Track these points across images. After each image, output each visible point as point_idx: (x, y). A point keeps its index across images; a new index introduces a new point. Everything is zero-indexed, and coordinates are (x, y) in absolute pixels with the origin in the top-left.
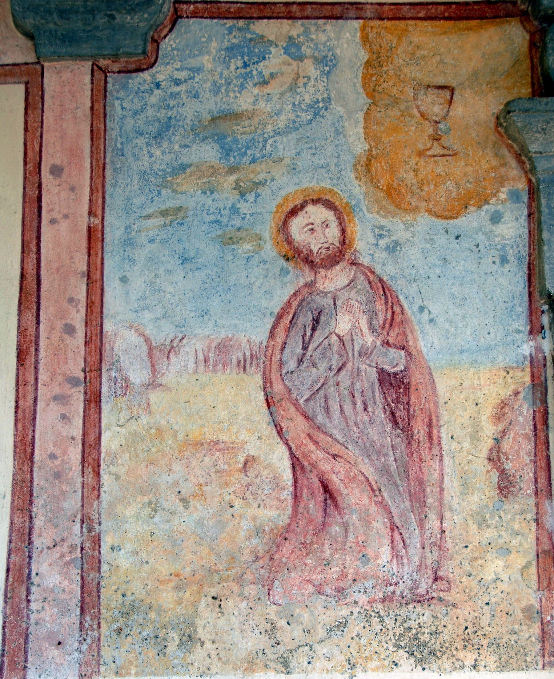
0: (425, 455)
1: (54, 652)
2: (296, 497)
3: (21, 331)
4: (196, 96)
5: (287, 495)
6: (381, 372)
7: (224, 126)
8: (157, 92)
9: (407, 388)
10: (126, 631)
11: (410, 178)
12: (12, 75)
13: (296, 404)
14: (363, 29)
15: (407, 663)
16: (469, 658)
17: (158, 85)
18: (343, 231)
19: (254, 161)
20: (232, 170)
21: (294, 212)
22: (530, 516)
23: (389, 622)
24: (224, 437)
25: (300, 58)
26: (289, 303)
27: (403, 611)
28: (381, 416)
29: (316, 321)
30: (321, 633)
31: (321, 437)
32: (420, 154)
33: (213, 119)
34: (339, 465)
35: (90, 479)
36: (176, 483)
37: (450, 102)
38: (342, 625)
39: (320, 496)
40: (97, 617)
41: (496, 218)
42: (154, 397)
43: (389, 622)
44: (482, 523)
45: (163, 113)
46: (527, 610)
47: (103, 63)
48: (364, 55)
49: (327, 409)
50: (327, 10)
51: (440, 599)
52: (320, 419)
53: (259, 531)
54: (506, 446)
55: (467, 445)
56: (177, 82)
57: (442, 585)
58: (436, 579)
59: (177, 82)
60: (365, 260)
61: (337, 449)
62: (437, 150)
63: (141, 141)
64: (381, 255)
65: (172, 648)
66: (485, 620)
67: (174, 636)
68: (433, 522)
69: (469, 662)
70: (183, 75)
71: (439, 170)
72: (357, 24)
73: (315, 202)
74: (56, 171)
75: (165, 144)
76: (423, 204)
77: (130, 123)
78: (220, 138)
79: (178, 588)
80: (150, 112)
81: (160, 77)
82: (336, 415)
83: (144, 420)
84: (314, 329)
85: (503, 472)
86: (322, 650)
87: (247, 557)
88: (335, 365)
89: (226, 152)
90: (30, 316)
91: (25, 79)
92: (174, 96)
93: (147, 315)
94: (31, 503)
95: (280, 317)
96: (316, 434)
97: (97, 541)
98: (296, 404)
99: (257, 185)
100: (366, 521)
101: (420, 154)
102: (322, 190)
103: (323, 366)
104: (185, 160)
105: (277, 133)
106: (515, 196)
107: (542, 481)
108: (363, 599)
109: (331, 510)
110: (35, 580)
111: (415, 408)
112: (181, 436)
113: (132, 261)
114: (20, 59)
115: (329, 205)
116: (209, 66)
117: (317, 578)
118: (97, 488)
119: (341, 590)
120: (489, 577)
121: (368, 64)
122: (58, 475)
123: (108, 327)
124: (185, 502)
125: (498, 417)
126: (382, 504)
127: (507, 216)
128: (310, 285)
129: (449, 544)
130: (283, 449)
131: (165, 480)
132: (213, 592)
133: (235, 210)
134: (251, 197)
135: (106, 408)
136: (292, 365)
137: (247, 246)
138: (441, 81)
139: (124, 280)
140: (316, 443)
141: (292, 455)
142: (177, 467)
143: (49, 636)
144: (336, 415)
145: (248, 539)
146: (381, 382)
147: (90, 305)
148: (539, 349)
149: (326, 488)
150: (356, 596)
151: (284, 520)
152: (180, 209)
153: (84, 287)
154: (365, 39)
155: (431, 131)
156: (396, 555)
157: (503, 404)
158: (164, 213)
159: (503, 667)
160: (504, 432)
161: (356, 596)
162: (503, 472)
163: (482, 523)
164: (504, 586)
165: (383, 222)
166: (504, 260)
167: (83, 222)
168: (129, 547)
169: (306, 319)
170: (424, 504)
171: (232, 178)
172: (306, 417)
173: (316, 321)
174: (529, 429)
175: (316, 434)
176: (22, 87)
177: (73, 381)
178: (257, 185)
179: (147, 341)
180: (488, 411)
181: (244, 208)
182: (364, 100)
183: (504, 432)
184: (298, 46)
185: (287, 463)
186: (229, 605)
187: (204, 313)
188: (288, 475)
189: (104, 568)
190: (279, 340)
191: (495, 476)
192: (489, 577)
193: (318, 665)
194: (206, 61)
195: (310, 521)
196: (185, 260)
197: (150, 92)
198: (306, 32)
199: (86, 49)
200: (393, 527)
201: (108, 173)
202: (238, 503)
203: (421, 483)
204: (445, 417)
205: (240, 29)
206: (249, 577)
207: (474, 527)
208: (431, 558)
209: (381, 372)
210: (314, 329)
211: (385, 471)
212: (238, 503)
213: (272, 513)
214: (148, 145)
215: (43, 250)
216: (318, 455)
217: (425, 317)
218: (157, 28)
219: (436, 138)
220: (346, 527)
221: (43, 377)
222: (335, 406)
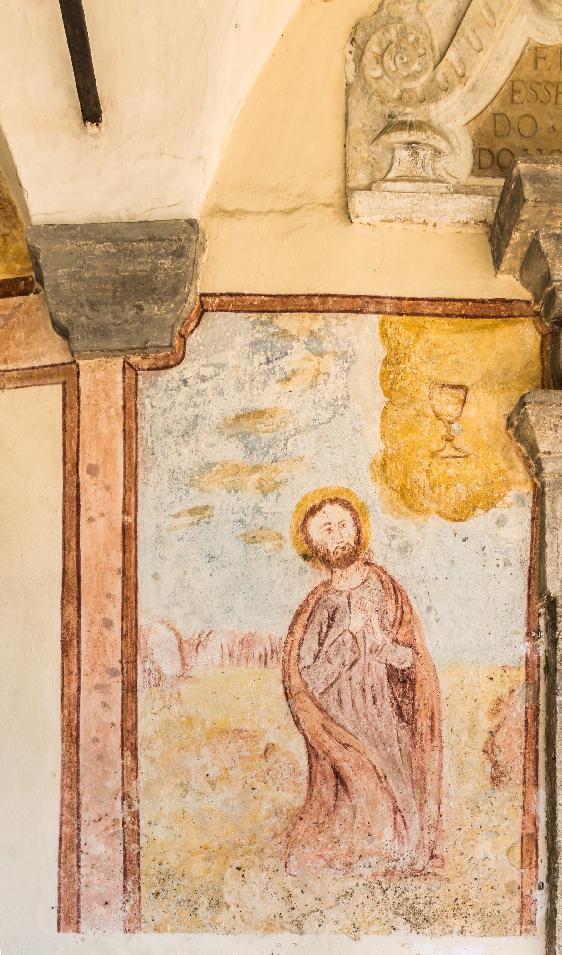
0: (427, 746)
1: (102, 910)
2: (311, 783)
3: (65, 625)
4: (221, 393)
5: (303, 779)
7: (246, 424)
8: (184, 389)
9: (413, 683)
10: (163, 894)
12: (51, 376)
13: (312, 697)
15: (403, 928)
16: (457, 924)
17: (185, 382)
19: (275, 460)
20: (256, 469)
21: (312, 512)
22: (518, 803)
24: (247, 727)
26: (307, 601)
28: (388, 709)
29: (332, 618)
30: (331, 901)
31: (334, 728)
32: (433, 455)
33: (238, 418)
34: (349, 754)
35: (129, 761)
36: (205, 767)
37: (464, 402)
38: (348, 894)
39: (332, 783)
40: (138, 882)
41: (501, 522)
42: (185, 687)
44: (476, 808)
47: (134, 359)
48: (382, 353)
49: (340, 702)
50: (346, 304)
52: (334, 711)
53: (277, 812)
55: (464, 737)
58: (432, 857)
59: (204, 379)
60: (378, 560)
62: (449, 451)
63: (170, 440)
64: (394, 556)
65: (202, 911)
66: (473, 893)
67: (204, 900)
68: (431, 807)
69: (457, 928)
70: (208, 372)
71: (451, 472)
72: (376, 319)
74: (92, 470)
75: (192, 442)
76: (434, 506)
77: (159, 420)
78: (244, 436)
80: (178, 410)
81: (187, 374)
83: (176, 708)
84: (329, 627)
85: (495, 764)
90: (71, 610)
91: (62, 379)
92: (200, 393)
94: (78, 781)
95: (298, 614)
96: (329, 725)
97: (136, 816)
98: (312, 697)
99: (278, 484)
100: (373, 804)
102: (340, 490)
103: (336, 661)
104: (212, 459)
106: (520, 500)
108: (367, 872)
109: (342, 794)
110: (83, 848)
111: (420, 703)
114: (58, 361)
115: (346, 505)
116: (233, 362)
118: (135, 770)
120: (479, 856)
121: (386, 362)
122: (100, 757)
123: (142, 621)
124: (212, 783)
125: (494, 712)
126: (386, 789)
128: (326, 584)
129: (445, 827)
130: (301, 738)
131: (193, 763)
133: (258, 510)
135: (141, 696)
136: (308, 660)
137: (269, 545)
138: (456, 380)
139: (156, 577)
140: (329, 733)
141: (308, 743)
143: (97, 896)
145: (268, 817)
146: (390, 677)
147: (125, 600)
149: (337, 774)
150: (363, 870)
151: (299, 802)
152: (206, 508)
153: (120, 583)
154: (384, 334)
155: (444, 431)
156: (398, 835)
157: (500, 701)
159: (485, 932)
161: (363, 870)
162: (495, 764)
163: (476, 808)
164: (491, 864)
167: (118, 518)
168: (164, 822)
169: (322, 616)
172: (321, 709)
173: (332, 618)
175: (329, 725)
176: (60, 387)
177: (113, 673)
178: (278, 484)
179: (178, 635)
180: (485, 706)
182: (381, 399)
184: (319, 341)
185: (303, 751)
186: (251, 875)
188: (303, 762)
190: (298, 635)
191: (488, 767)
193: (327, 927)
199: (116, 343)
200: (396, 811)
201: (140, 472)
202: (259, 786)
203: (422, 771)
204: (446, 711)
205: (263, 324)
206: (268, 851)
207: (467, 812)
208: (428, 838)
210: (329, 627)
211: (390, 760)
212: (259, 786)
213: (290, 796)
215: (82, 548)
216: (330, 744)
217: (432, 614)
218: (185, 324)
220: (354, 810)
221: (85, 667)
222: (347, 699)
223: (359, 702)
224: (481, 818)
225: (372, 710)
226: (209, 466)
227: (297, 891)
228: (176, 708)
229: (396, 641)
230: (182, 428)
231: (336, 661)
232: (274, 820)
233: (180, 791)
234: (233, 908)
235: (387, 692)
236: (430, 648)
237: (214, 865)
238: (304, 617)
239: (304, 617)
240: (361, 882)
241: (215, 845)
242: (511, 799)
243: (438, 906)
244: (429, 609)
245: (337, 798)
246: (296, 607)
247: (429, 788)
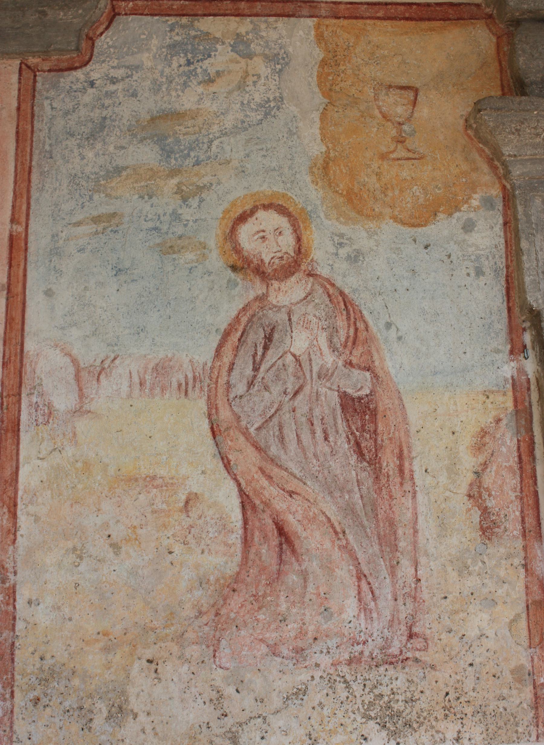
0: (396, 491)
2: (246, 542)
5: (236, 538)
6: (344, 397)
8: (90, 91)
9: (374, 414)
10: (44, 701)
11: (372, 182)
13: (246, 433)
14: (317, 27)
18: (299, 239)
20: (174, 172)
21: (243, 218)
23: (357, 688)
24: (162, 472)
25: (250, 56)
27: (373, 675)
29: (269, 339)
30: (276, 702)
32: (383, 157)
33: (153, 119)
34: (296, 504)
36: (106, 525)
37: (414, 103)
39: (275, 541)
43: (357, 688)
45: (96, 114)
46: (517, 671)
47: (32, 61)
48: (319, 54)
49: (282, 439)
51: (417, 660)
52: (274, 450)
53: (203, 582)
54: (488, 480)
55: (443, 479)
56: (114, 81)
57: (418, 643)
58: (411, 636)
59: (114, 81)
60: (324, 271)
61: (293, 485)
62: (404, 154)
63: (72, 143)
65: (99, 722)
66: (469, 684)
70: (120, 73)
71: (405, 174)
72: (310, 22)
73: (266, 207)
75: (99, 146)
76: (388, 211)
79: (106, 650)
80: (83, 112)
81: (95, 76)
82: (292, 445)
83: (69, 451)
84: (266, 348)
85: (485, 511)
86: (277, 722)
87: (188, 612)
88: (291, 389)
89: (167, 153)
92: (109, 95)
93: (75, 333)
95: (227, 334)
98: (246, 433)
99: (201, 189)
101: (383, 157)
102: (275, 195)
104: (120, 162)
105: (224, 134)
106: (488, 203)
107: (530, 521)
108: (325, 661)
109: (288, 555)
111: (383, 438)
112: (112, 471)
113: (59, 272)
115: (282, 211)
117: (272, 636)
119: (299, 651)
120: (473, 633)
121: (323, 63)
123: (30, 346)
126: (346, 548)
127: (481, 224)
128: (261, 299)
129: (425, 595)
130: (231, 485)
132: (148, 654)
133: (176, 216)
134: (194, 202)
136: (240, 388)
138: (403, 81)
139: (49, 293)
140: (269, 478)
141: (242, 492)
142: (106, 506)
144: (292, 445)
145: (190, 590)
146: (344, 407)
148: (521, 371)
149: (281, 531)
151: (232, 568)
152: (114, 215)
154: (320, 38)
156: (364, 608)
157: (484, 433)
158: (96, 220)
160: (485, 465)
162: (485, 511)
164: (490, 644)
165: (343, 229)
166: (479, 272)
168: (49, 600)
170: (395, 548)
171: (174, 181)
173: (269, 339)
174: (513, 461)
178: (201, 189)
179: (74, 361)
181: (186, 213)
182: (319, 100)
183: (485, 465)
184: (247, 44)
185: (236, 501)
187: (140, 330)
188: (236, 516)
189: (20, 625)
190: (227, 359)
192: (473, 633)
194: (146, 59)
195: (263, 569)
196: (119, 271)
197: (84, 91)
198: (256, 29)
200: (360, 576)
201: (34, 177)
202: (178, 549)
203: (392, 523)
204: (417, 447)
208: (404, 612)
209: (344, 397)
210: (266, 348)
213: (219, 560)
214: (79, 146)
219: (400, 141)
220: (304, 576)
222: (290, 436)
223: (306, 437)
224: (472, 582)
225: (323, 448)
226: (118, 170)
227: (231, 690)
228: (69, 451)
229: (349, 364)
230: (86, 130)
231: (276, 389)
232: (198, 593)
233: (72, 557)
234: (142, 717)
235: (341, 425)
236: (392, 372)
237: (117, 658)
238: (235, 337)
239: (235, 337)
240: (318, 674)
241: (118, 630)
242: (509, 556)
243: (423, 704)
244: (388, 325)
245: (281, 561)
246: (223, 326)
247: (402, 544)
